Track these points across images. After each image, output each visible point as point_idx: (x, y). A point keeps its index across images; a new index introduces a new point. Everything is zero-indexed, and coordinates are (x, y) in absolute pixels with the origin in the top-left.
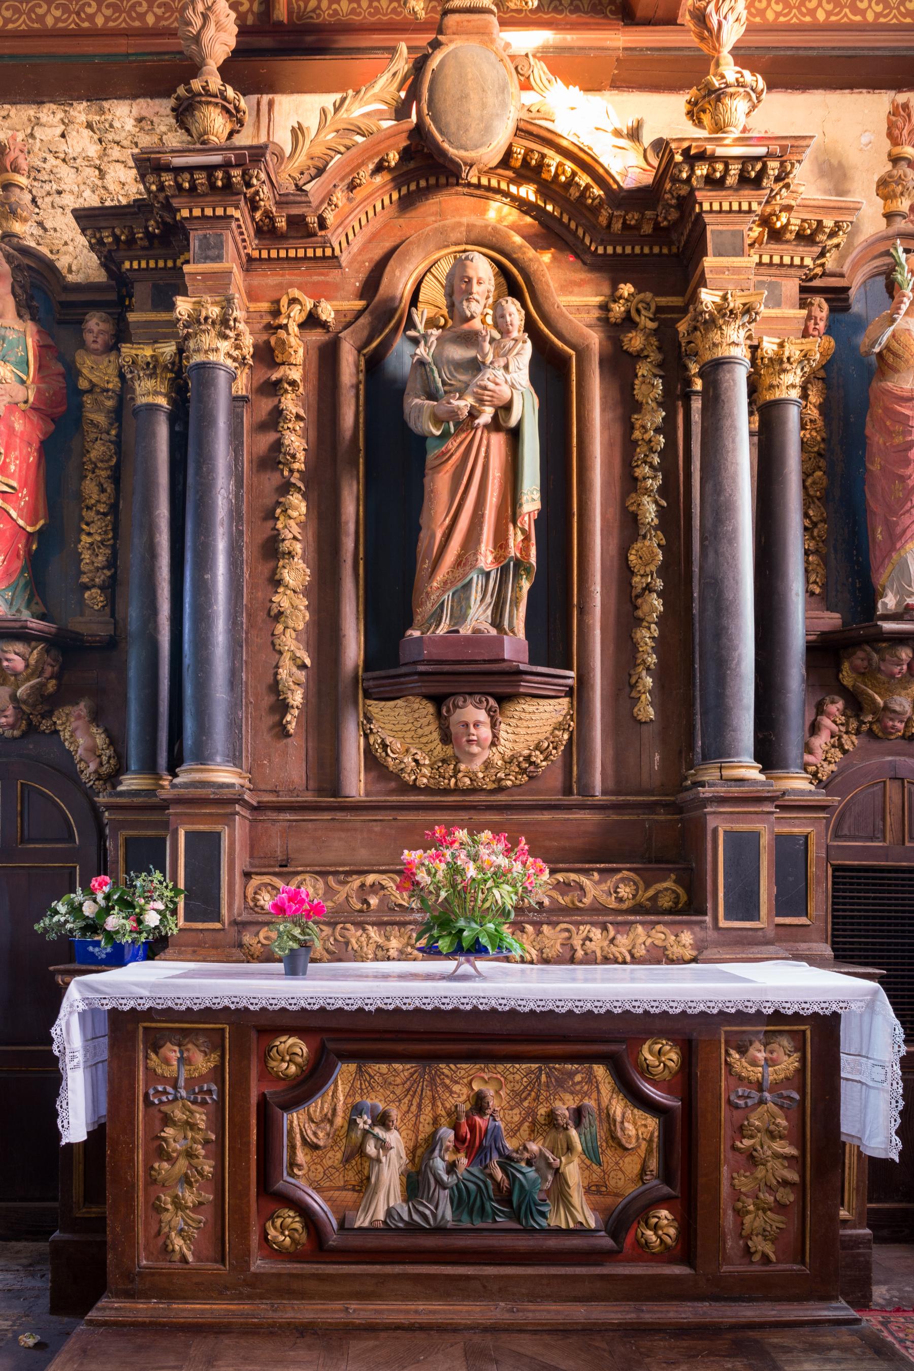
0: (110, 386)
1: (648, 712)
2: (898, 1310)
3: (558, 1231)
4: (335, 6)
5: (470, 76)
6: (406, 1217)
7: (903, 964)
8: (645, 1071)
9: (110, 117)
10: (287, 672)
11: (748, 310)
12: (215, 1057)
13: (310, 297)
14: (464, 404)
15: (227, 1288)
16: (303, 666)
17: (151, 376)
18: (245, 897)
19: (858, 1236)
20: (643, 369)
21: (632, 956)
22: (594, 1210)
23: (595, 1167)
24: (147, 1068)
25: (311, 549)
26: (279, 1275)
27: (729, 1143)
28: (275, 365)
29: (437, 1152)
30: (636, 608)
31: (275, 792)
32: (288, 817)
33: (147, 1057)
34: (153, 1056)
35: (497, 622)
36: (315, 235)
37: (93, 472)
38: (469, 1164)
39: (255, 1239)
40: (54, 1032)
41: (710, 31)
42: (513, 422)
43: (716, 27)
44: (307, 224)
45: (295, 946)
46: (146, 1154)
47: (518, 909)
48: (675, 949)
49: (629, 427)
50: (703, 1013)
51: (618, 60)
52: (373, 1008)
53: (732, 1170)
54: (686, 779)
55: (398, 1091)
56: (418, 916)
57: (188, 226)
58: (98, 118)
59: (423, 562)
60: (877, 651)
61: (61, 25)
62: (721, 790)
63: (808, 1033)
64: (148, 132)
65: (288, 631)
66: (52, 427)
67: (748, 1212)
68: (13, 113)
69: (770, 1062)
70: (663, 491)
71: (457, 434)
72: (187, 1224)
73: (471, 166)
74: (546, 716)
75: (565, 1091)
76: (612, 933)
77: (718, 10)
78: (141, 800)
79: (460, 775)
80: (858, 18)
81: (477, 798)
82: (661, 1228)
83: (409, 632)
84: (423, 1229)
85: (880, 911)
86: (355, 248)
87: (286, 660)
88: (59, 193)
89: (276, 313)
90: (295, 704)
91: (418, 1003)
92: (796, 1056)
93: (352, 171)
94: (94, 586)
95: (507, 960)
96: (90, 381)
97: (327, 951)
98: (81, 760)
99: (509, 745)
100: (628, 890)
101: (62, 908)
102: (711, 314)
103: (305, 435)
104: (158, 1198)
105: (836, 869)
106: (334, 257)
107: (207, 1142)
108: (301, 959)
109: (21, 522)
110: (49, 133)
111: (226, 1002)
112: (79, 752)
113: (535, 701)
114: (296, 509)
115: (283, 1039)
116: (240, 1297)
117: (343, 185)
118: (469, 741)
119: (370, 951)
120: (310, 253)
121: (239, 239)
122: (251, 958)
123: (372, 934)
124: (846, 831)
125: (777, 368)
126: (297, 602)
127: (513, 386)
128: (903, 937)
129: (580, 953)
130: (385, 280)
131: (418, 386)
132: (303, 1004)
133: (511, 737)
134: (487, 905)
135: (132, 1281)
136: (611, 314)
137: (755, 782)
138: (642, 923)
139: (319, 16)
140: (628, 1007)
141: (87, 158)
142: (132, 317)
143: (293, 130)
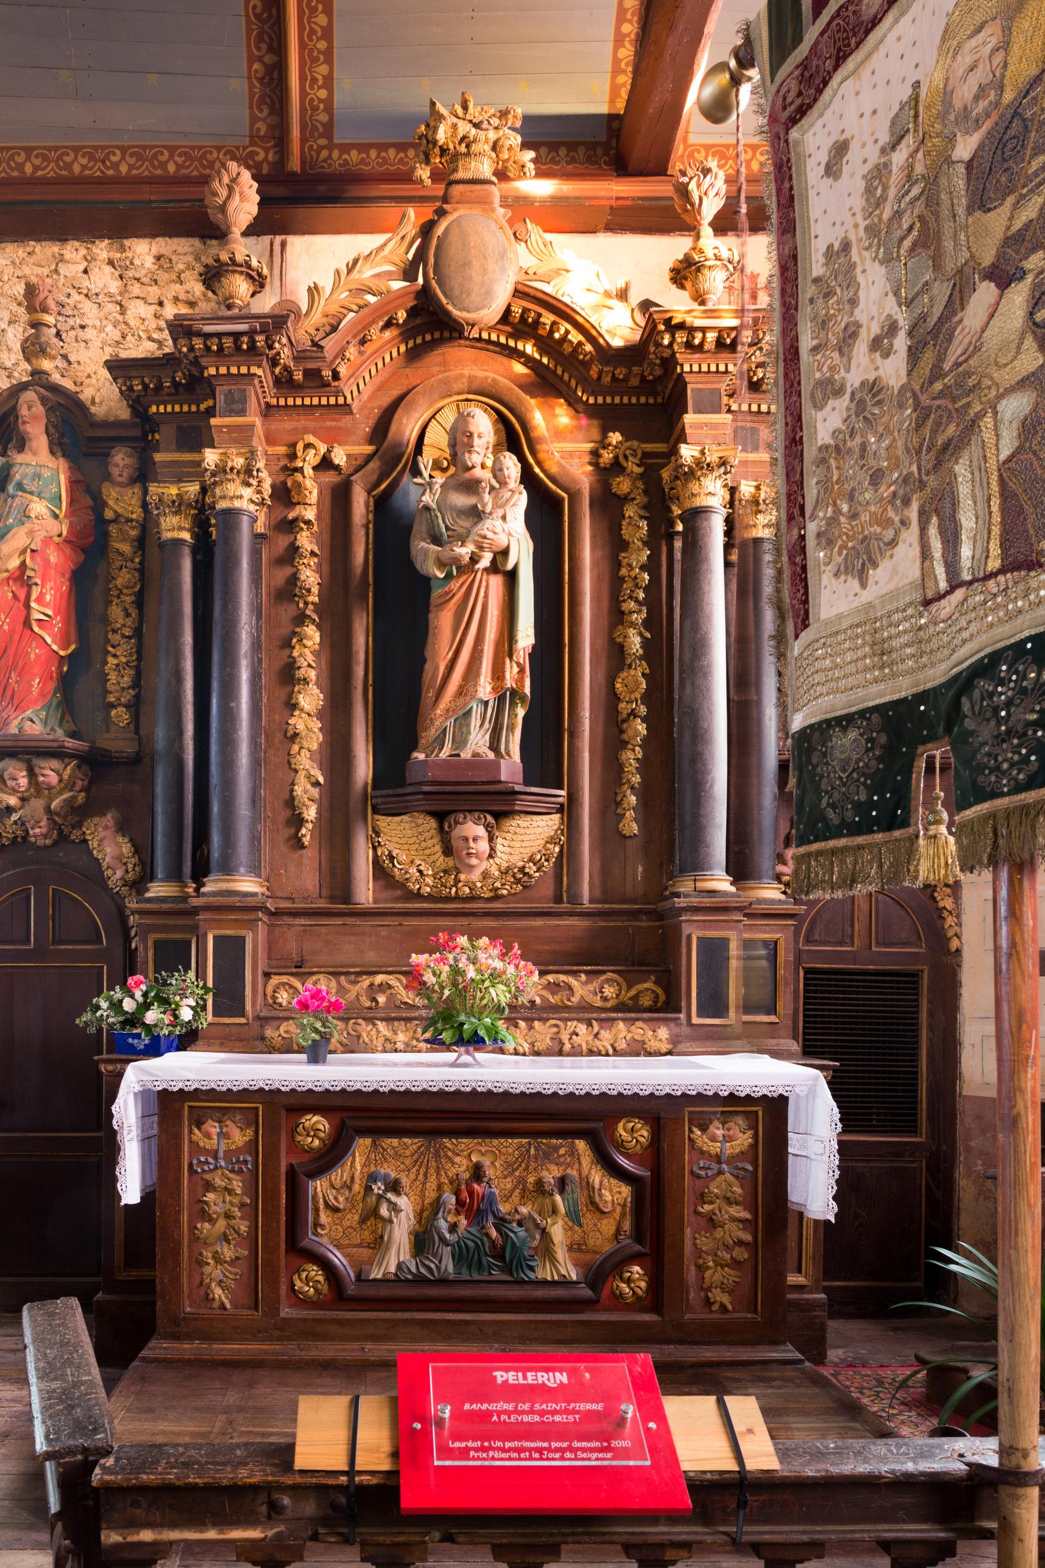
0: (134, 516)
1: (631, 826)
2: (850, 1366)
3: (545, 1283)
4: (345, 156)
5: (472, 244)
6: (414, 1270)
7: (870, 1060)
8: (620, 1146)
9: (130, 255)
10: (303, 790)
11: (723, 462)
12: (250, 1132)
13: (324, 442)
14: (464, 551)
15: (259, 1331)
16: (316, 784)
17: (176, 513)
18: (265, 995)
19: (814, 1299)
20: (630, 511)
21: (614, 1049)
22: (575, 1265)
23: (576, 1228)
24: (190, 1141)
25: (325, 675)
26: (305, 1320)
27: (692, 1208)
28: (291, 504)
29: (440, 1214)
30: (622, 732)
31: (289, 899)
32: (303, 921)
33: (191, 1132)
34: (196, 1131)
35: (494, 746)
36: (329, 385)
38: (469, 1225)
39: (283, 1289)
40: (114, 1109)
41: (692, 205)
42: (510, 566)
43: (697, 202)
44: (322, 377)
45: (317, 1037)
46: (190, 1216)
47: (512, 1007)
48: (652, 1043)
49: (617, 565)
50: (668, 1095)
51: (611, 208)
52: (386, 1090)
53: (695, 1231)
54: (666, 888)
55: (407, 1162)
56: (423, 1013)
57: (214, 382)
58: (118, 255)
59: (428, 691)
61: (87, 172)
62: (695, 901)
63: (760, 1113)
64: (166, 270)
65: (303, 751)
66: (82, 557)
67: (708, 1268)
68: (38, 249)
69: (727, 1139)
70: (647, 624)
71: (459, 576)
72: (225, 1276)
73: (473, 326)
74: (539, 830)
75: (551, 1162)
78: (169, 905)
79: (460, 885)
81: (475, 906)
82: (634, 1281)
83: (415, 754)
84: (430, 1280)
86: (365, 396)
87: (301, 778)
88: (83, 327)
89: (293, 456)
90: (310, 818)
91: (425, 1086)
92: (750, 1133)
93: (364, 328)
95: (502, 1051)
96: (116, 512)
97: (341, 1043)
101: (104, 1005)
102: (690, 467)
103: (319, 570)
104: (201, 1254)
105: (808, 971)
106: (346, 405)
107: (243, 1205)
108: (321, 1052)
109: (55, 647)
110: (72, 270)
111: (261, 1085)
112: (107, 859)
113: (529, 817)
114: (310, 638)
115: (308, 1117)
116: (271, 1339)
117: (355, 341)
118: (469, 854)
119: (379, 1044)
120: (324, 401)
121: (260, 391)
122: (272, 1049)
123: (381, 1029)
124: (817, 937)
126: (311, 725)
127: (510, 534)
128: (883, 1036)
129: (567, 1047)
130: (393, 427)
131: (424, 530)
132: (327, 1086)
134: (484, 1002)
135: (178, 1325)
136: (601, 460)
137: (725, 894)
138: (623, 1020)
139: (330, 165)
140: (604, 1089)
141: (110, 295)
142: (158, 457)
143: (309, 289)
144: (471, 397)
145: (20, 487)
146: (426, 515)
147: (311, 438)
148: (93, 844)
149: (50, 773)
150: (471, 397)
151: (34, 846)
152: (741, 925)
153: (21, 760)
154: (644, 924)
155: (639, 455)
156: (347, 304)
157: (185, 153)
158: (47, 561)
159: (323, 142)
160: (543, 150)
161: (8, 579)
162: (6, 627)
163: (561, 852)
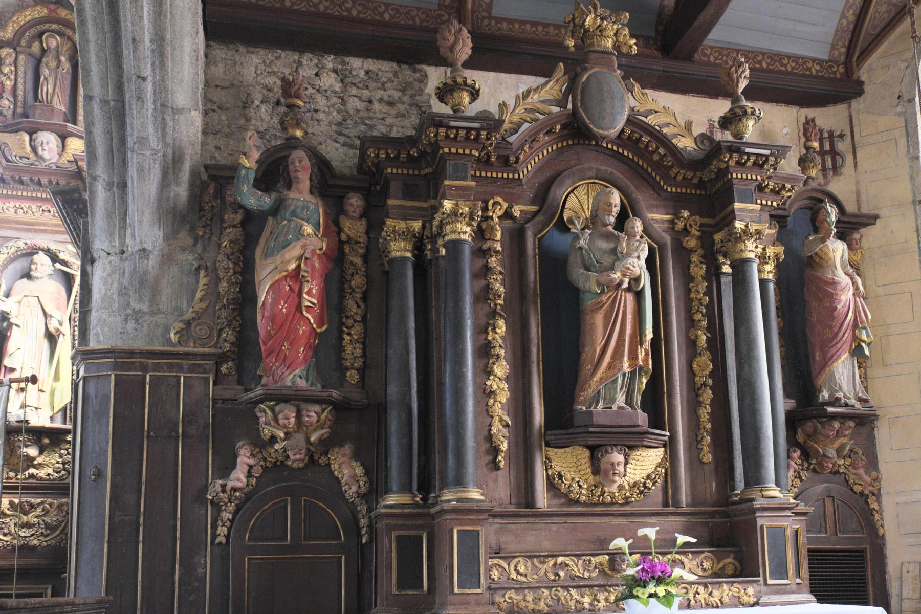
0: (361, 240)
1: (708, 457)
4: (499, 25)
5: (605, 89)
16: (507, 426)
20: (695, 258)
21: (722, 603)
30: (698, 395)
36: (511, 166)
37: (350, 294)
58: (340, 67)
60: (820, 423)
65: (496, 404)
68: (283, 55)
73: (604, 138)
76: (710, 590)
77: (736, 72)
78: (408, 510)
80: (783, 68)
85: (826, 575)
88: (316, 111)
94: (353, 368)
98: (346, 484)
99: (632, 476)
100: (708, 564)
103: (503, 283)
110: (307, 72)
112: (345, 478)
114: (501, 328)
118: (614, 474)
126: (502, 386)
133: (633, 471)
138: (726, 583)
141: (335, 92)
143: (500, 105)
144: (596, 181)
145: (294, 214)
146: (579, 253)
147: (499, 199)
148: (335, 466)
149: (312, 414)
150: (596, 181)
151: (290, 468)
152: (791, 519)
153: (291, 404)
154: (719, 520)
155: (699, 224)
156: (524, 117)
157: (396, 9)
158: (313, 267)
159: (484, 14)
160: (641, 40)
161: (286, 277)
162: (284, 310)
163: (666, 473)
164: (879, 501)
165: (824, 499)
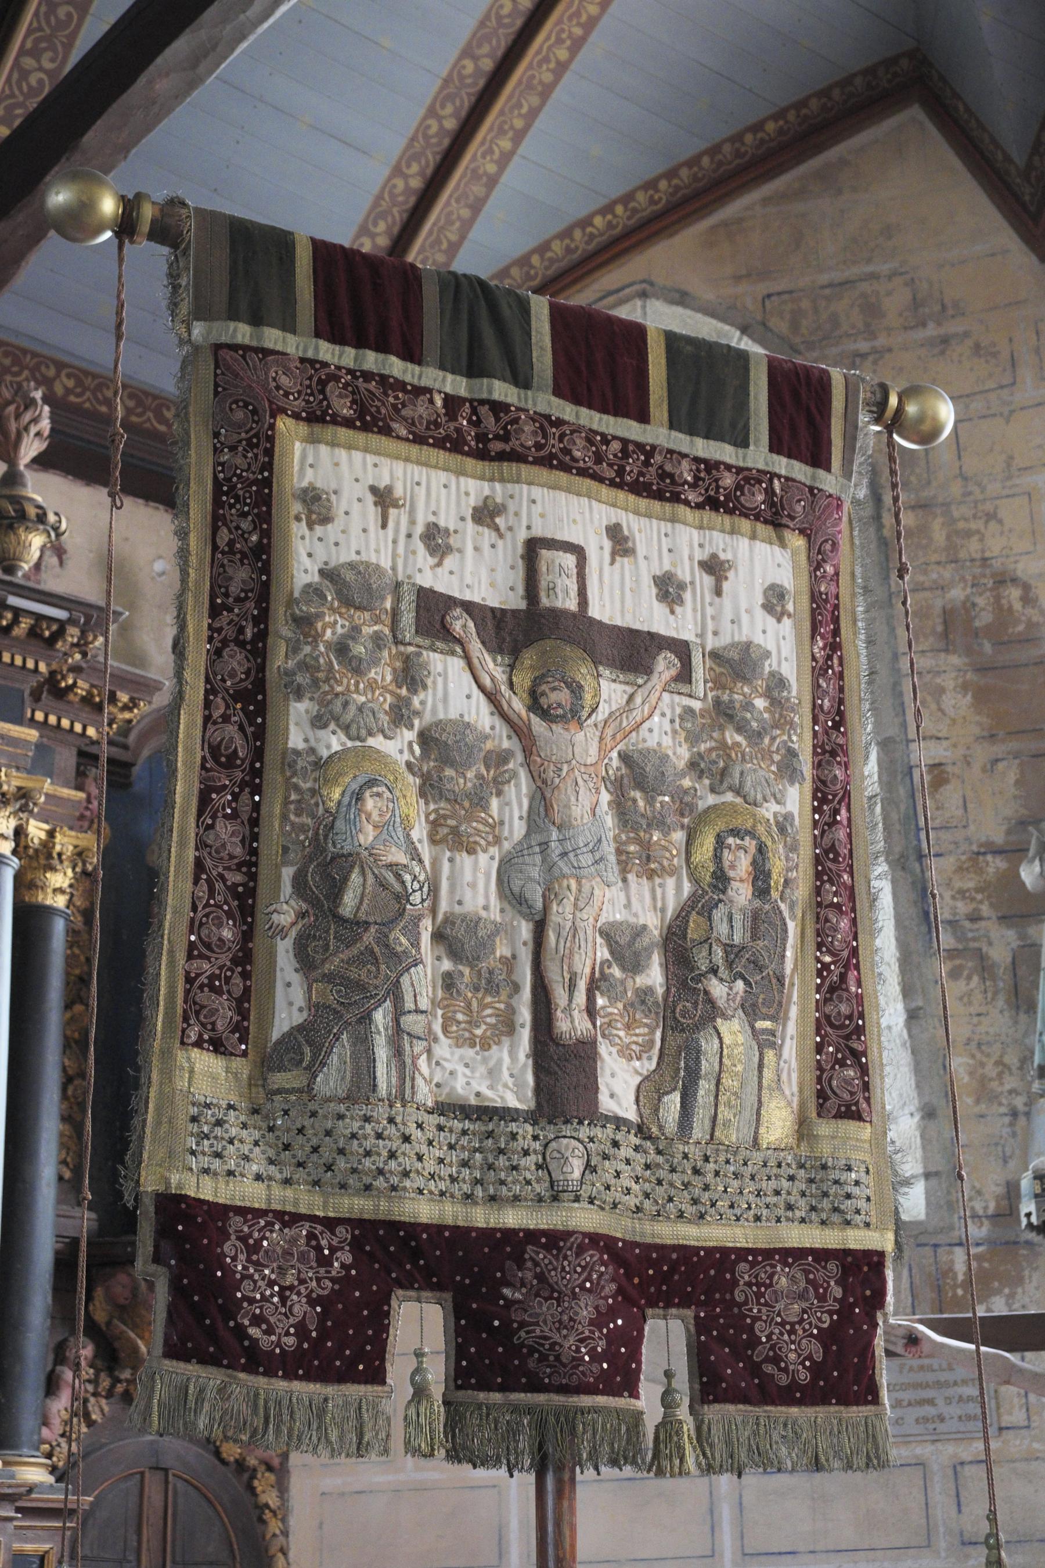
43: (13, 436)
77: (18, 416)
125: (43, 862)
152: (10, 1526)
164: (282, 1487)
165: (142, 1474)
